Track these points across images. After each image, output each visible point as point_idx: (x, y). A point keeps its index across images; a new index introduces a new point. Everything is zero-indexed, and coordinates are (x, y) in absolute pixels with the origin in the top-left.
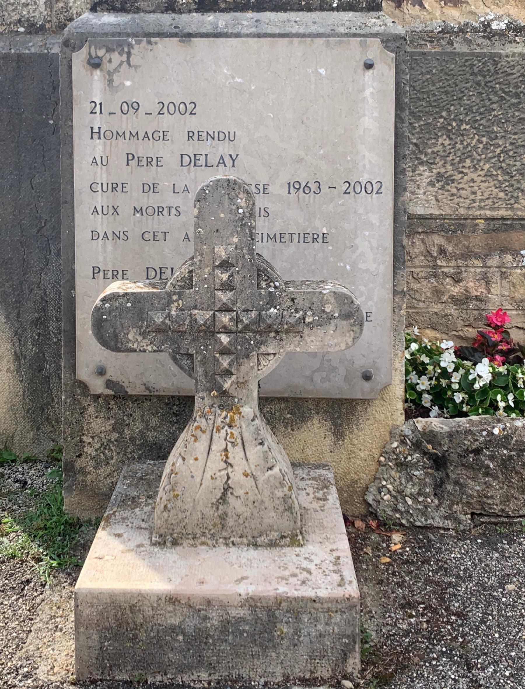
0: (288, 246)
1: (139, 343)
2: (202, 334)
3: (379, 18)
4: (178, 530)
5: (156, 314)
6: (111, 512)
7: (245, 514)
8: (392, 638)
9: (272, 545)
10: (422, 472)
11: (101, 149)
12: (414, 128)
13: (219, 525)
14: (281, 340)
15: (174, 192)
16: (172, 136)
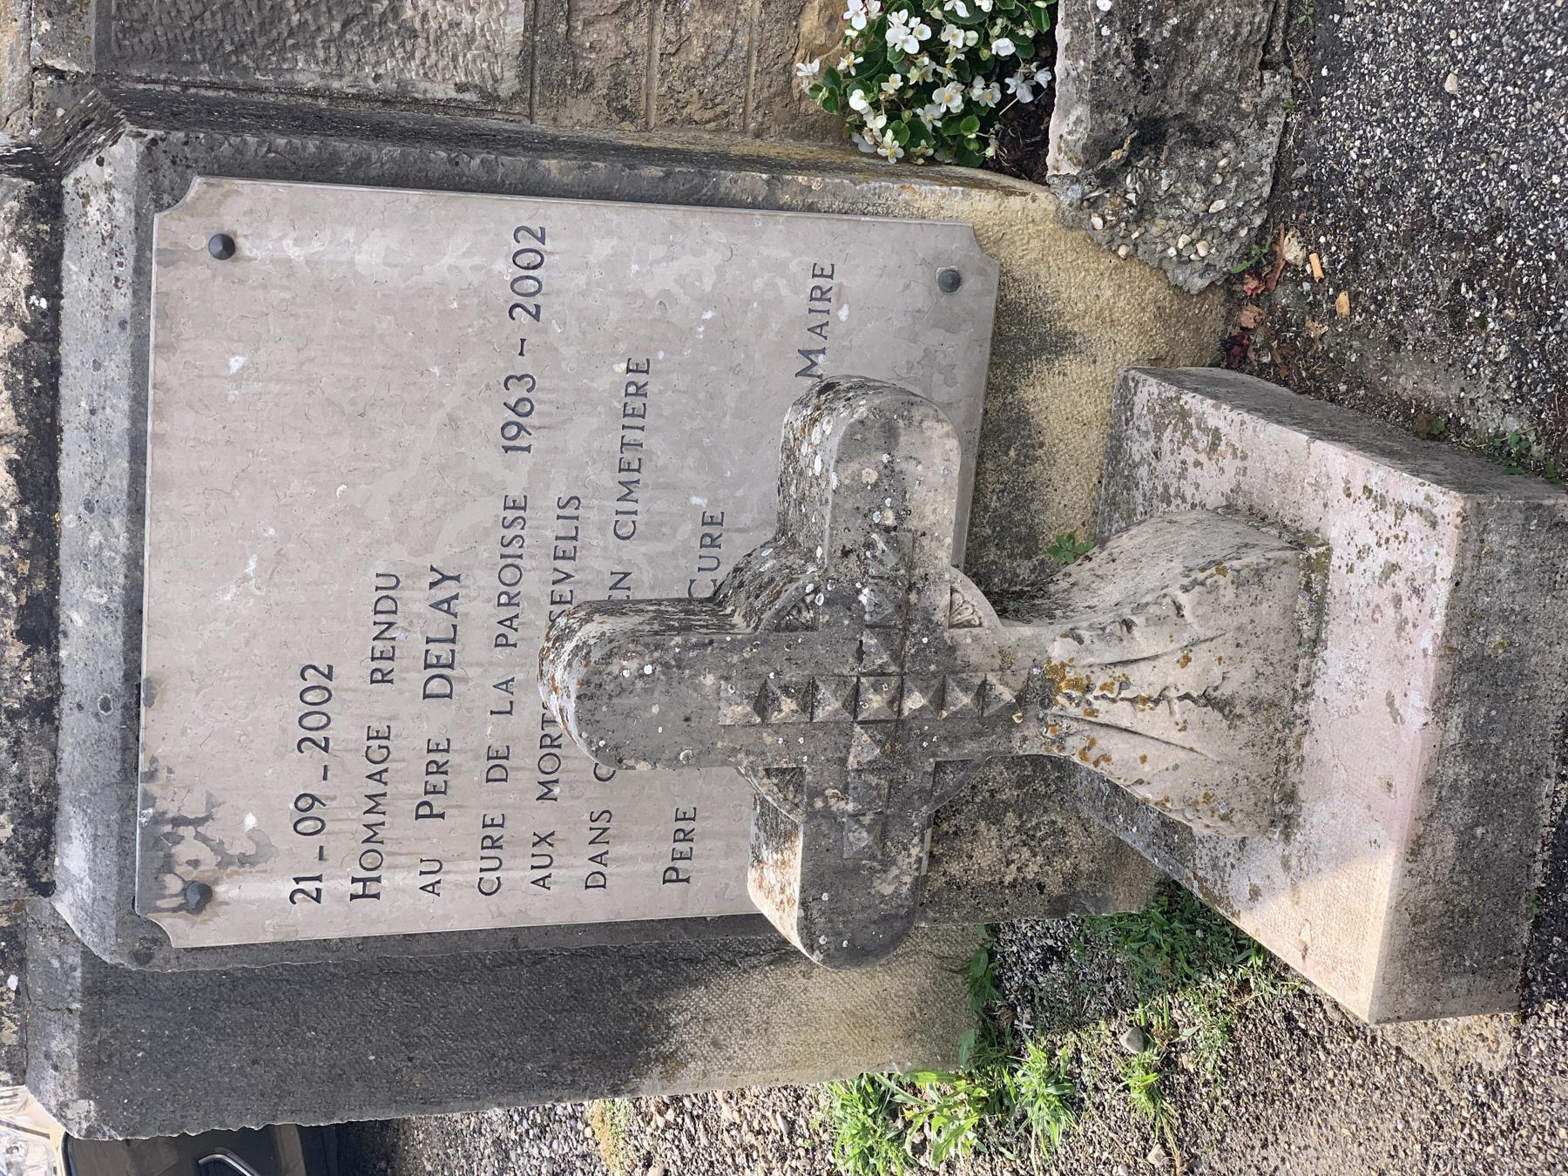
0: (650, 453)
1: (902, 873)
2: (898, 747)
3: (86, 197)
4: (1267, 791)
5: (851, 844)
6: (1196, 884)
7: (1258, 662)
8: (1525, 389)
9: (1319, 609)
10: (1164, 172)
11: (404, 874)
12: (303, 24)
13: (1270, 720)
14: (926, 577)
15: (510, 713)
16: (380, 719)
